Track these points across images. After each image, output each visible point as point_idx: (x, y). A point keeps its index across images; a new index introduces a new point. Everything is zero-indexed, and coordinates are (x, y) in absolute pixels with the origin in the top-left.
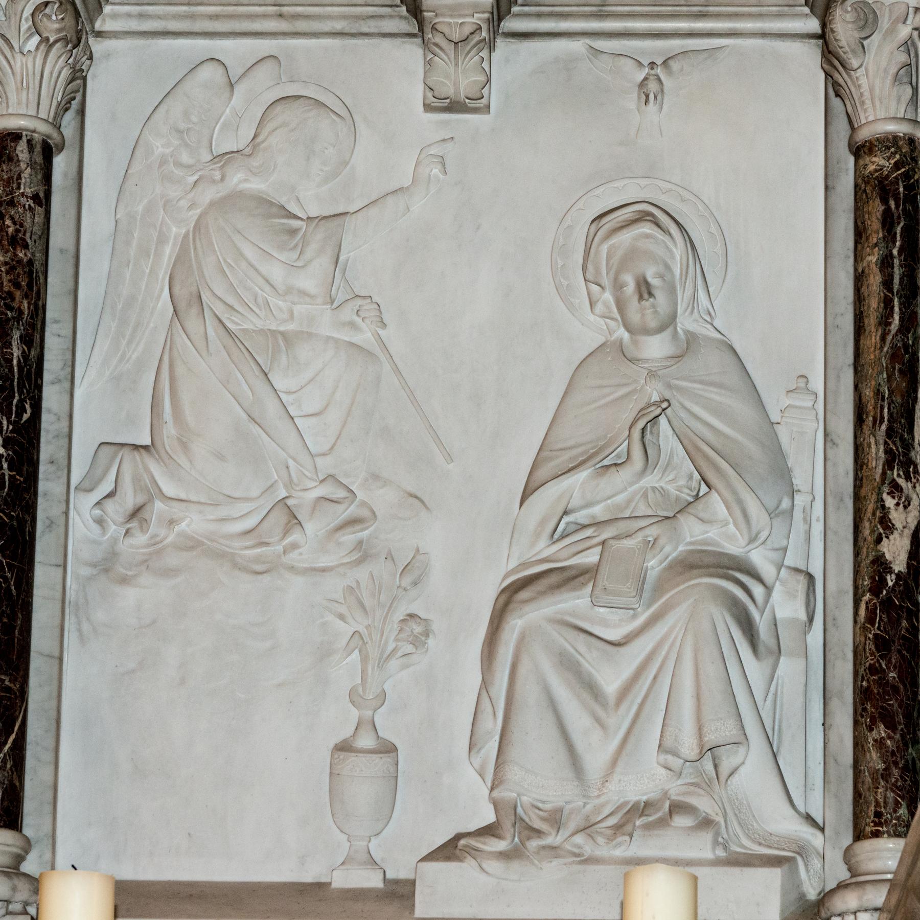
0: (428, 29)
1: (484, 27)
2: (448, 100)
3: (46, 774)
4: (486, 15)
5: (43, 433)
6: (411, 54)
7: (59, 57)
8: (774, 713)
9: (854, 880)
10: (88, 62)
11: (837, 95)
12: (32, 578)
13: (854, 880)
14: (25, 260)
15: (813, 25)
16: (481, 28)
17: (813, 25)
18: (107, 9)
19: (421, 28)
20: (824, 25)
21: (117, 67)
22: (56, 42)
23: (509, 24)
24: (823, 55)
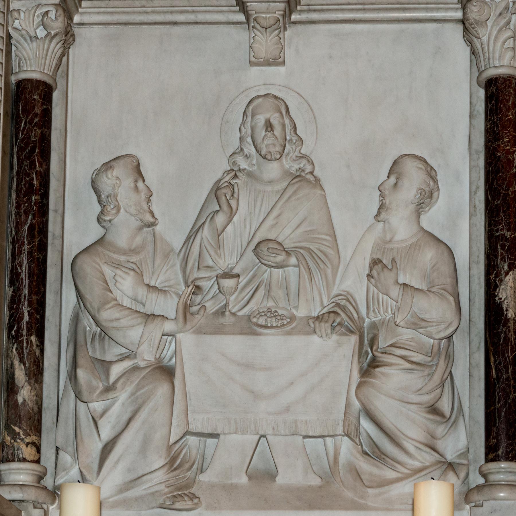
0: (252, 20)
1: (281, 18)
2: (262, 60)
3: (58, 242)
4: (282, 12)
5: (47, 305)
6: (241, 35)
7: (57, 44)
8: (443, 375)
9: (487, 484)
10: (72, 42)
11: (473, 54)
12: (50, 140)
13: (487, 484)
14: (36, 256)
15: (459, 15)
16: (279, 20)
17: (459, 15)
18: (84, 4)
19: (248, 17)
20: (464, 14)
21: (89, 42)
22: (56, 35)
23: (294, 17)
24: (464, 30)
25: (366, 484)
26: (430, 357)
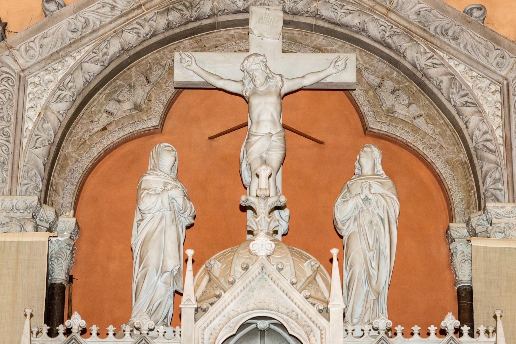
25: (155, 122)
26: (181, 89)
